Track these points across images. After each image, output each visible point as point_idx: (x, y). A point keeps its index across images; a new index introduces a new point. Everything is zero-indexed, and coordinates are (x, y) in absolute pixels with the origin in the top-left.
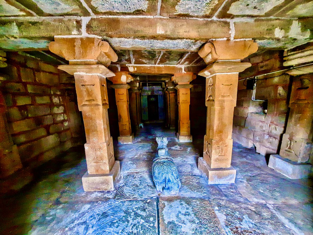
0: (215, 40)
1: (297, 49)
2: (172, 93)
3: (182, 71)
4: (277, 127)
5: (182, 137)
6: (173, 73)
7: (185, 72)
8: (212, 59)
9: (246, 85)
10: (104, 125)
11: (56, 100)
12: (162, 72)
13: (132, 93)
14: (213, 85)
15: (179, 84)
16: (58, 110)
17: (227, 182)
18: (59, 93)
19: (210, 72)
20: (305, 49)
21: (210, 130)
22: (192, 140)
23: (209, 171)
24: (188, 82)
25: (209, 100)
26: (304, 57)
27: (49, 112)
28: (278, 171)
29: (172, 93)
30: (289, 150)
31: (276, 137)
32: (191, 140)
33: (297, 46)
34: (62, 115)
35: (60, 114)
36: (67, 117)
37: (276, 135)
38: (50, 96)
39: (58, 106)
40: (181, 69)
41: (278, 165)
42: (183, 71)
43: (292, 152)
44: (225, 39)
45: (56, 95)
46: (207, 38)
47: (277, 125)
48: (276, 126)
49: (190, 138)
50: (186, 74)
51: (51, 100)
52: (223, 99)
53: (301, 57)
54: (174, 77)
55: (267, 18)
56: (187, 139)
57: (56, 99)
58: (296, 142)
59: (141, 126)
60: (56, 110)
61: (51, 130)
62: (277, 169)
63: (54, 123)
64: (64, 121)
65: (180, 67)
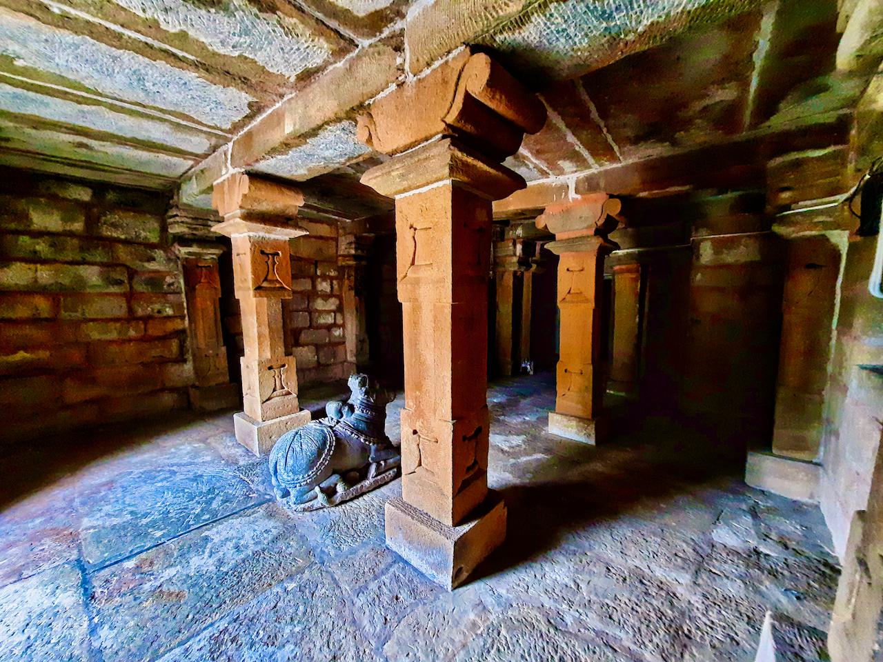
0: (374, 101)
2: (621, 272)
3: (567, 194)
5: (557, 417)
6: (539, 205)
7: (579, 197)
9: (859, 214)
10: (259, 326)
11: (324, 286)
12: (507, 208)
13: (505, 272)
15: (558, 237)
16: (324, 306)
18: (333, 274)
22: (593, 436)
24: (589, 227)
26: (167, 123)
27: (304, 306)
29: (621, 272)
32: (589, 436)
34: (333, 314)
35: (329, 312)
38: (313, 279)
39: (326, 297)
40: (566, 188)
42: (572, 194)
44: (393, 87)
45: (324, 277)
49: (586, 429)
50: (584, 200)
51: (314, 286)
52: (417, 276)
54: (543, 216)
56: (575, 430)
57: (324, 284)
59: (526, 368)
60: (320, 304)
61: (303, 337)
63: (311, 327)
64: (335, 325)
65: (559, 183)
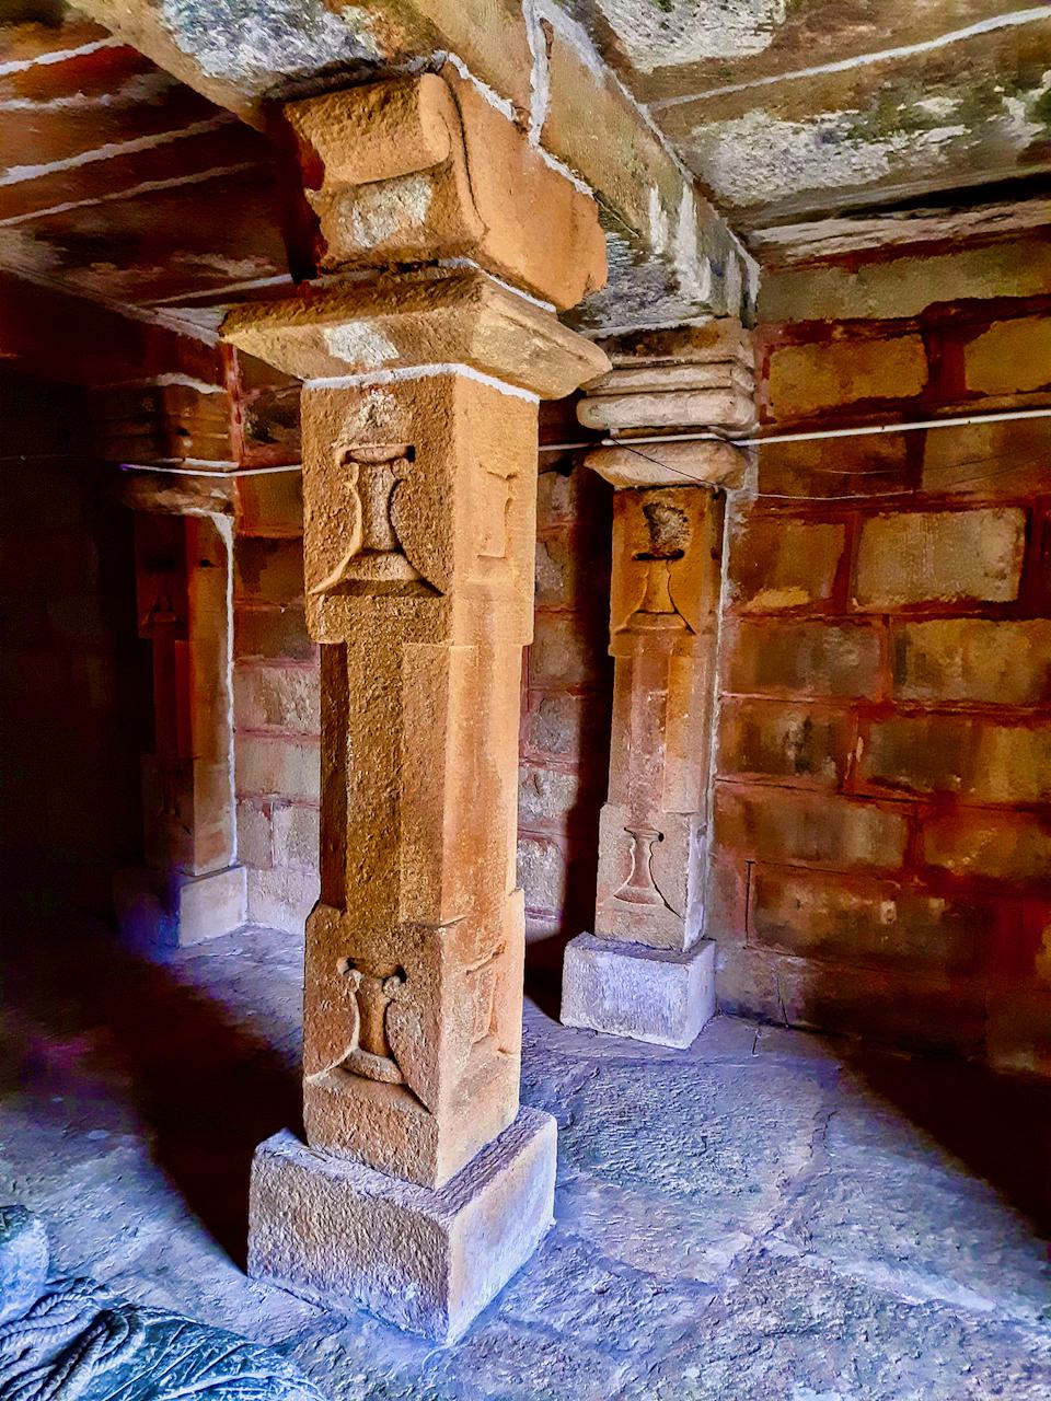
1: (640, 347)
4: (541, 772)
8: (430, 229)
14: (410, 454)
17: (527, 1239)
19: (400, 336)
20: (669, 353)
21: (389, 842)
23: (442, 1220)
25: (348, 588)
26: (668, 396)
28: (619, 1031)
30: (635, 889)
31: (545, 832)
33: (637, 327)
36: (958, 776)
37: (541, 824)
41: (615, 995)
43: (651, 901)
46: (446, 31)
47: (541, 764)
48: (535, 769)
53: (657, 393)
55: (44, 106)
58: (661, 837)
62: (612, 1018)
